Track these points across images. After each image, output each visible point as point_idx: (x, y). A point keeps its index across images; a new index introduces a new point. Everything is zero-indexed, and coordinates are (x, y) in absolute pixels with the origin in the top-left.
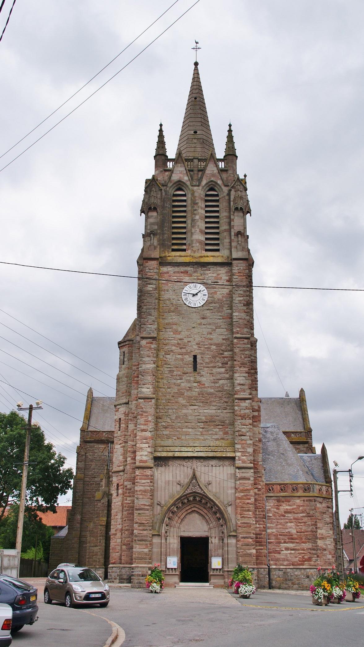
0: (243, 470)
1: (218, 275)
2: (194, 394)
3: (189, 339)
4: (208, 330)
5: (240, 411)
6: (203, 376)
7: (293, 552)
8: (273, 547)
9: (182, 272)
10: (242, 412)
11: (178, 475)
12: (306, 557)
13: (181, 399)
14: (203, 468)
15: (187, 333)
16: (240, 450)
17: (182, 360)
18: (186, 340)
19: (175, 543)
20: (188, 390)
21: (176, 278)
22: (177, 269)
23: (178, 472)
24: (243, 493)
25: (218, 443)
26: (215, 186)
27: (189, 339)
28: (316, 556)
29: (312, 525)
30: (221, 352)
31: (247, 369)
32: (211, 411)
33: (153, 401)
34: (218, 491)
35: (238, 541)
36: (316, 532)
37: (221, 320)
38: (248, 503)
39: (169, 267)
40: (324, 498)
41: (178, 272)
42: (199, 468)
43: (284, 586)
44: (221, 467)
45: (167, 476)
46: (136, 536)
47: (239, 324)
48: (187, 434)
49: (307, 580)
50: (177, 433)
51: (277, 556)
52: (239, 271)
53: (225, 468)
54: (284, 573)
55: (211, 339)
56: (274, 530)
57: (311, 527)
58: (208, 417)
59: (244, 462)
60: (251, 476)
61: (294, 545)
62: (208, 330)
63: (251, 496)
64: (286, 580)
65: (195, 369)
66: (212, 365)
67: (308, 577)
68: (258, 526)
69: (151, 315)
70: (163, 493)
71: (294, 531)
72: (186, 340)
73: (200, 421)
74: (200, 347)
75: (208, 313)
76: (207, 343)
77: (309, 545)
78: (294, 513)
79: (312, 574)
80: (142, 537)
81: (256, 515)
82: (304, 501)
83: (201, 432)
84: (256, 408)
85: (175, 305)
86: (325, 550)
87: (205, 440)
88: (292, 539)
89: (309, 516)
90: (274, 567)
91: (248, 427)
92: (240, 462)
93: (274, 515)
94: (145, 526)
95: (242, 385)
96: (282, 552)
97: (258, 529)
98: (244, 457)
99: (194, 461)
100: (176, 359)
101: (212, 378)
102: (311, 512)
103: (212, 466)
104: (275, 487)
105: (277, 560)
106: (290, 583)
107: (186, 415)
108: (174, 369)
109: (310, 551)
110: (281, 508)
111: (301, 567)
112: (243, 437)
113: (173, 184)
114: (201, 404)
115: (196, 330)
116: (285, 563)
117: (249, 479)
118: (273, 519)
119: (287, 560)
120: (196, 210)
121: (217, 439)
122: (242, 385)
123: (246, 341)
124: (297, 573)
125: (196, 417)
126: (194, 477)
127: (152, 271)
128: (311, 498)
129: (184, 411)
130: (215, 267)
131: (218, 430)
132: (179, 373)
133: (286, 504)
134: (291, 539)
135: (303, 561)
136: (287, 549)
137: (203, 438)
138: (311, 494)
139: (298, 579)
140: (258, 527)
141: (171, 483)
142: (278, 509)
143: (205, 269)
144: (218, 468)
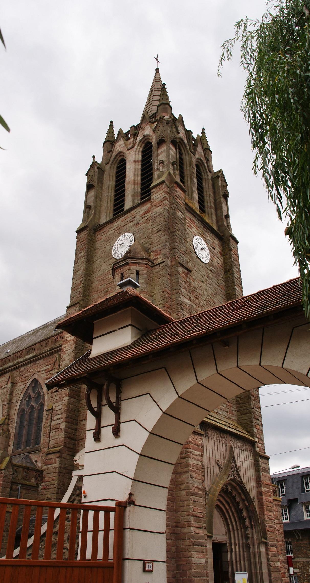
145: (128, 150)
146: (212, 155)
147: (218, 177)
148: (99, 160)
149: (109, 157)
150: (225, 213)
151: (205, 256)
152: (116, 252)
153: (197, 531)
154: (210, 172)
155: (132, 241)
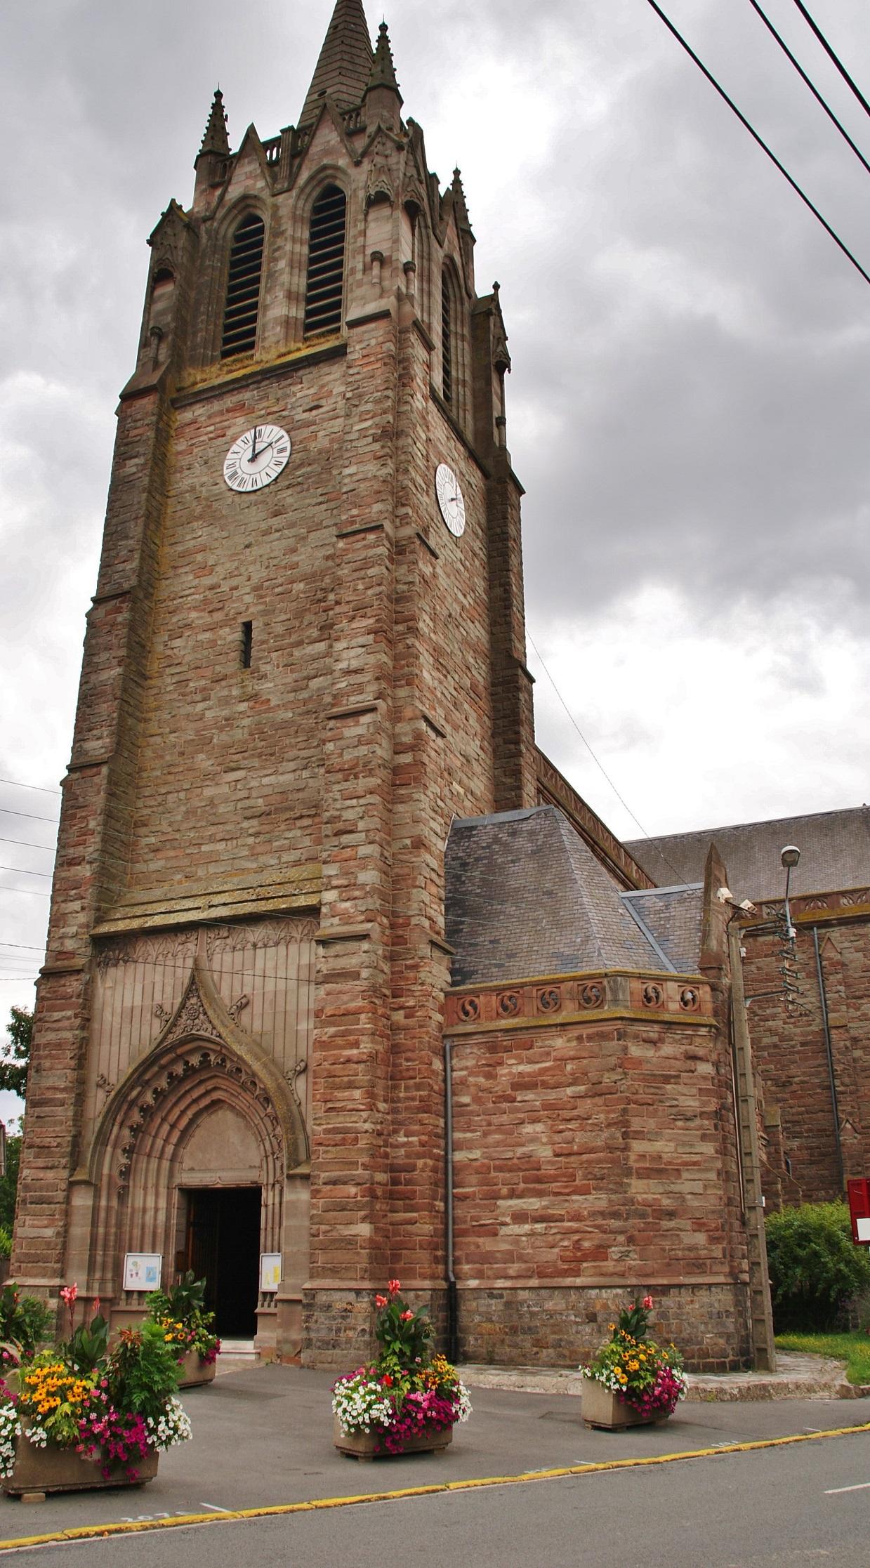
0: (338, 948)
1: (323, 386)
2: (239, 734)
3: (234, 582)
4: (285, 543)
5: (341, 755)
6: (264, 676)
7: (539, 1227)
8: (473, 1212)
9: (228, 411)
10: (347, 756)
11: (158, 988)
12: (586, 1244)
13: (202, 756)
14: (228, 957)
15: (230, 566)
16: (335, 882)
17: (213, 643)
18: (225, 587)
19: (155, 1205)
20: (221, 729)
21: (212, 428)
22: (217, 406)
23: (158, 978)
24: (333, 1024)
25: (293, 873)
26: (335, 177)
27: (234, 582)
28: (621, 1238)
29: (609, 1125)
30: (320, 595)
31: (371, 621)
32: (282, 778)
33: (105, 770)
34: (268, 1026)
35: (315, 1194)
36: (626, 1149)
37: (324, 507)
38: (349, 1061)
39: (198, 406)
40: (670, 1025)
41: (221, 413)
42: (217, 958)
43: (505, 1351)
44: (282, 948)
45: (128, 994)
46: (27, 1188)
47: (357, 496)
48: (213, 859)
49: (588, 1329)
50: (186, 862)
51: (486, 1244)
52: (365, 352)
53: (293, 948)
54: (508, 1304)
55: (294, 566)
56: (476, 1154)
57: (605, 1134)
58: (273, 799)
59: (346, 919)
60: (361, 965)
61: (545, 1202)
62: (285, 543)
63: (362, 1032)
64: (514, 1330)
65: (246, 661)
66: (294, 638)
67: (592, 1318)
68: (403, 1139)
69: (127, 537)
70: (115, 1049)
71: (545, 1153)
72: (225, 587)
73: (248, 813)
74: (262, 597)
75: (288, 497)
76: (280, 581)
77: (598, 1200)
78: (545, 1085)
79: (605, 1306)
80: (41, 1189)
81: (399, 1100)
82: (579, 1038)
83: (252, 848)
84: (407, 739)
85: (207, 499)
86: (671, 1215)
87: (261, 870)
88: (539, 1180)
89: (597, 1092)
90: (473, 1283)
91: (362, 801)
92: (336, 920)
93: (477, 1100)
94: (50, 1155)
95: (356, 672)
96: (504, 1231)
97: (402, 1151)
98: (348, 904)
99: (204, 936)
100: (199, 646)
101: (290, 678)
102: (608, 1079)
103: (255, 946)
104: (481, 1001)
105: (487, 1258)
106: (527, 1342)
107: (212, 803)
108: (190, 675)
109: (600, 1221)
110: (502, 1071)
111: (568, 1281)
112: (346, 839)
113: (230, 210)
114: (256, 763)
115: (255, 551)
116: (513, 1269)
117: (356, 976)
118: (471, 1113)
119: (521, 1259)
120: (279, 248)
121: (296, 863)
122: (356, 672)
123: (371, 537)
124: (554, 1303)
125: (240, 805)
126: (194, 986)
127: (139, 424)
128: (606, 1028)
129: (208, 792)
130: (314, 370)
131: (299, 833)
132: (203, 682)
133: (518, 1057)
134: (534, 1178)
135: (575, 1260)
136: (520, 1217)
137: (254, 865)
138: (606, 1011)
139: (558, 1328)
140: (404, 1145)
141: (137, 1013)
142: (489, 1076)
143: (289, 381)
144: (271, 951)
145: (274, 195)
146: (475, 247)
147: (489, 313)
148: (187, 204)
149: (214, 203)
150: (496, 414)
151: (456, 516)
152: (236, 473)
153: (41, 1174)
154: (469, 296)
155: (283, 450)
